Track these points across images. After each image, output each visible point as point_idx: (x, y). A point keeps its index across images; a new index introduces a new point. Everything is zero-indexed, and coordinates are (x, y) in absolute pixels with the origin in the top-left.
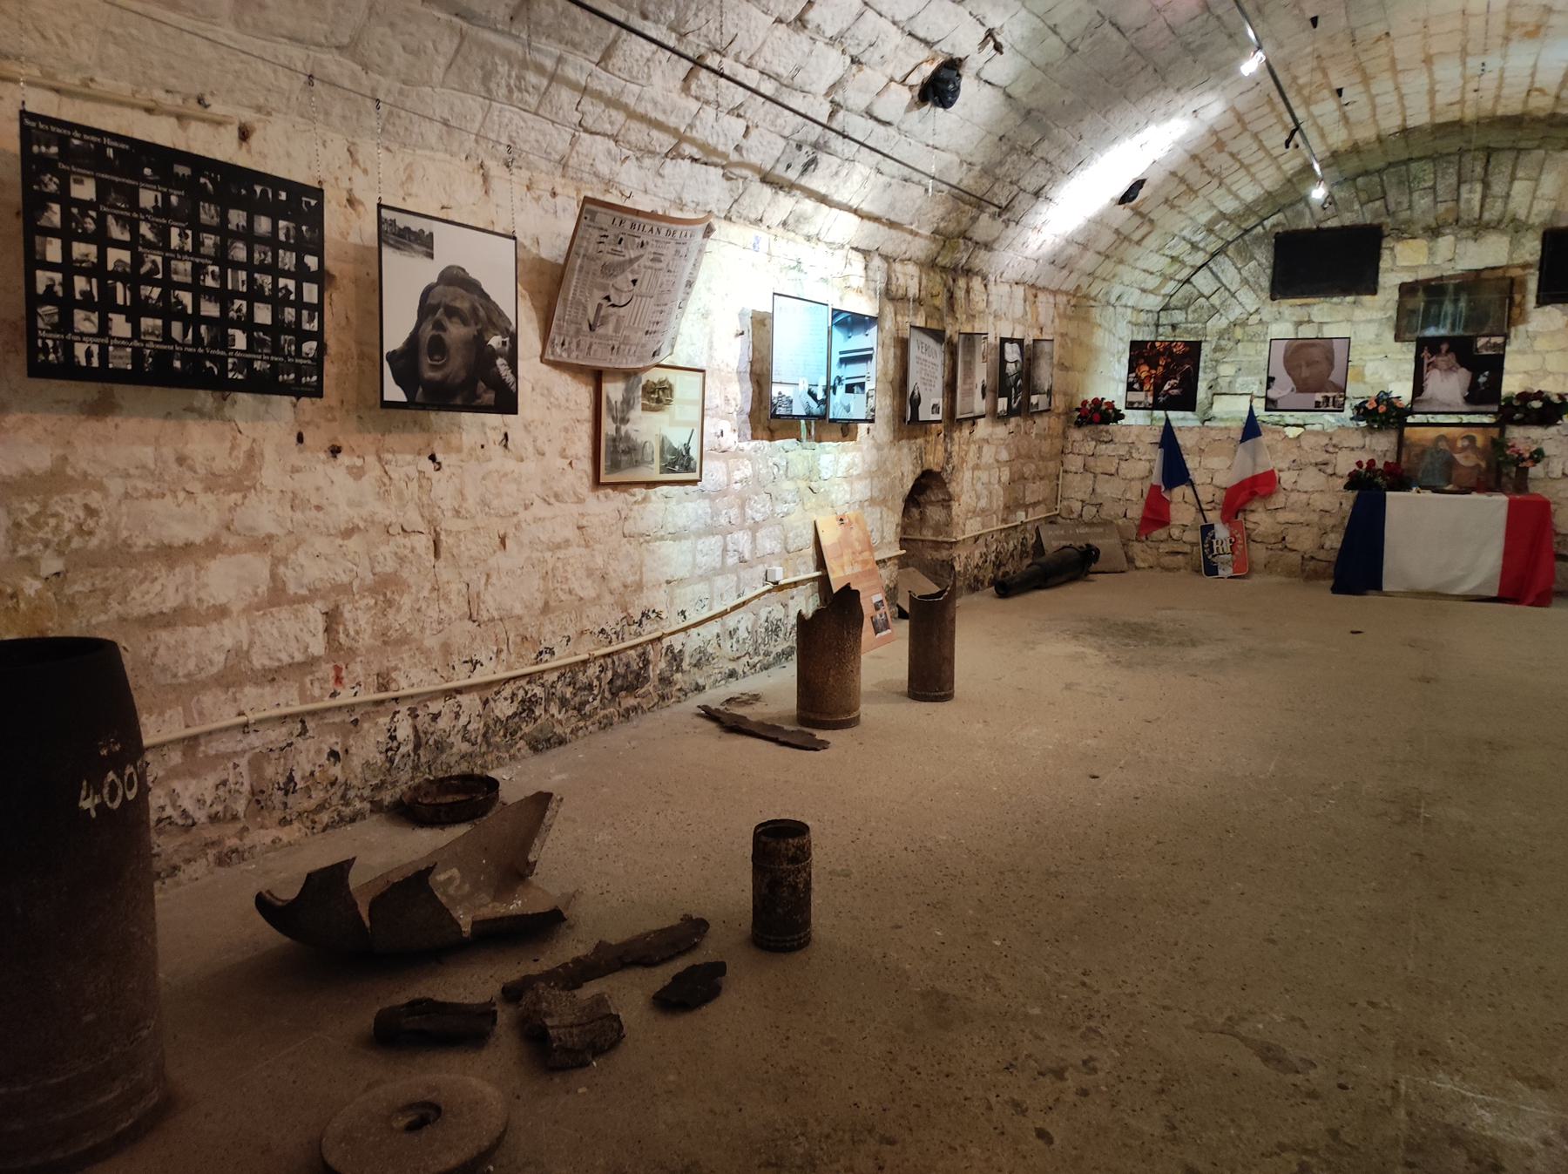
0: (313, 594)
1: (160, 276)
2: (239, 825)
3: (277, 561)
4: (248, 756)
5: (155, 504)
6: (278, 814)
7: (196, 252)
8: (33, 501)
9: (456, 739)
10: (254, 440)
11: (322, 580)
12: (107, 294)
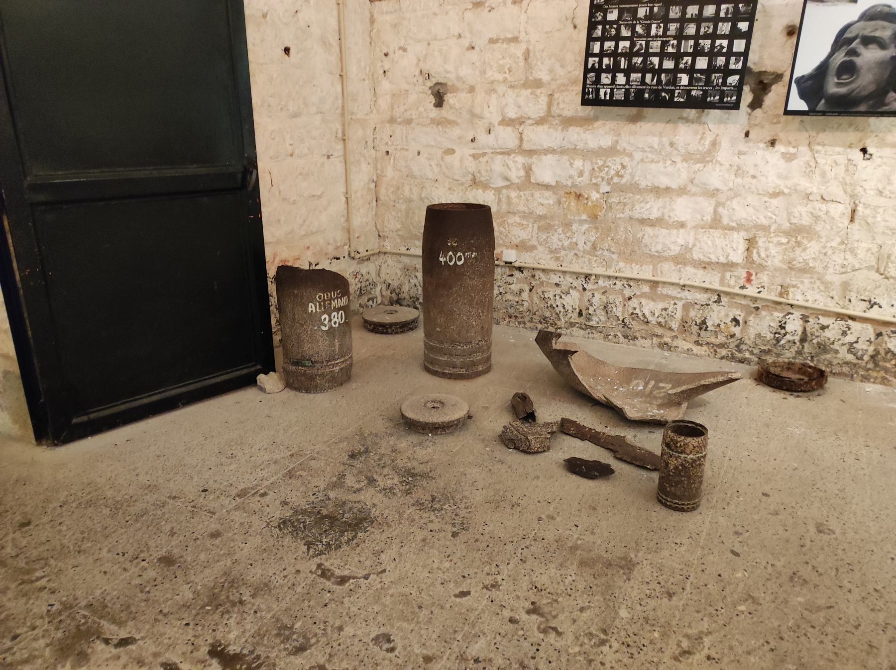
0: (739, 227)
1: (643, 51)
2: (674, 334)
3: (718, 204)
4: (683, 302)
5: (653, 167)
6: (695, 338)
7: (665, 35)
8: (601, 160)
9: (843, 352)
10: (717, 135)
11: (746, 220)
12: (617, 63)
